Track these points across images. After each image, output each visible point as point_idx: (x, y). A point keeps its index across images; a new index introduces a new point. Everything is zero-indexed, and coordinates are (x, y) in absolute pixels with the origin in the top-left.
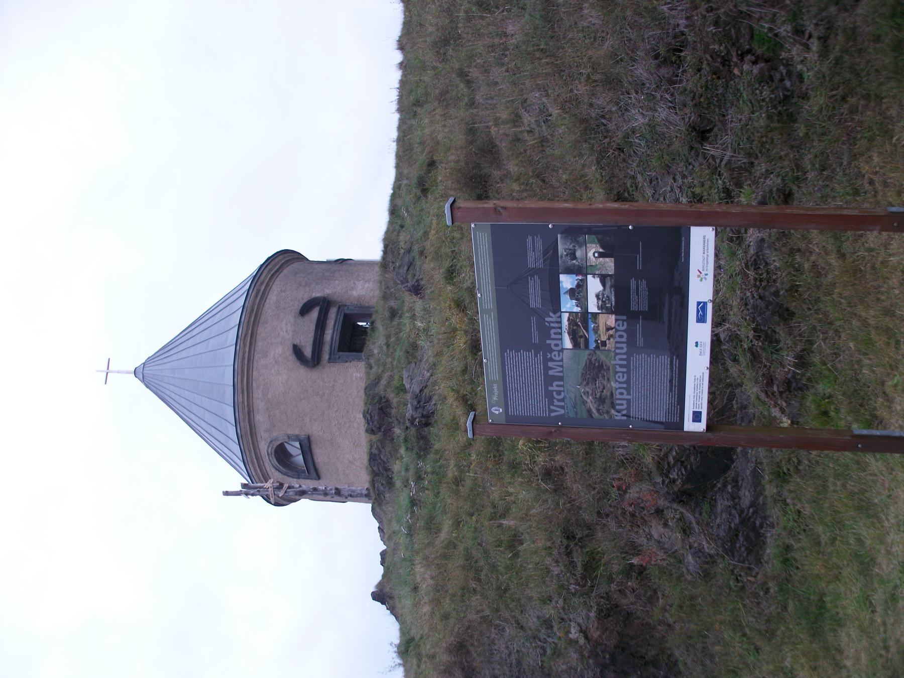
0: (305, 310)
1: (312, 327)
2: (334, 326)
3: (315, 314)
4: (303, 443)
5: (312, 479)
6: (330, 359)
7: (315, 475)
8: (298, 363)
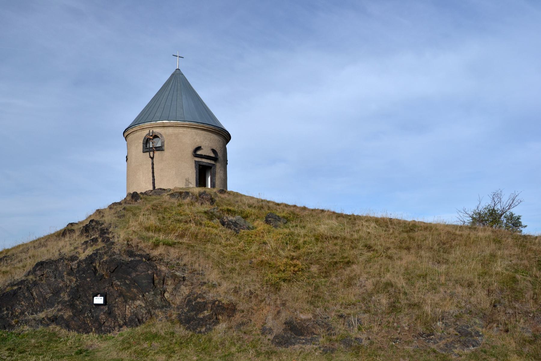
0: (214, 151)
1: (207, 154)
2: (208, 163)
3: (212, 155)
4: (160, 148)
5: (143, 149)
6: (196, 161)
7: (145, 151)
8: (194, 148)
